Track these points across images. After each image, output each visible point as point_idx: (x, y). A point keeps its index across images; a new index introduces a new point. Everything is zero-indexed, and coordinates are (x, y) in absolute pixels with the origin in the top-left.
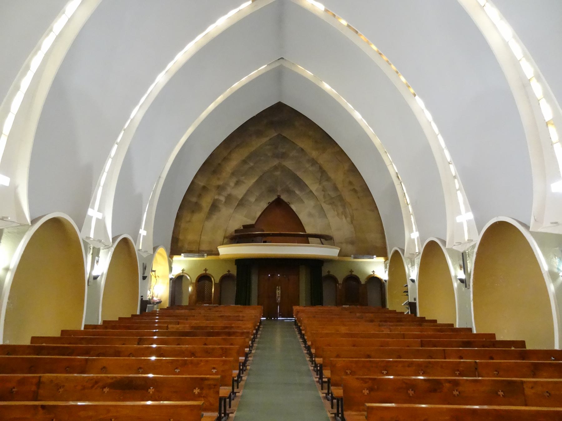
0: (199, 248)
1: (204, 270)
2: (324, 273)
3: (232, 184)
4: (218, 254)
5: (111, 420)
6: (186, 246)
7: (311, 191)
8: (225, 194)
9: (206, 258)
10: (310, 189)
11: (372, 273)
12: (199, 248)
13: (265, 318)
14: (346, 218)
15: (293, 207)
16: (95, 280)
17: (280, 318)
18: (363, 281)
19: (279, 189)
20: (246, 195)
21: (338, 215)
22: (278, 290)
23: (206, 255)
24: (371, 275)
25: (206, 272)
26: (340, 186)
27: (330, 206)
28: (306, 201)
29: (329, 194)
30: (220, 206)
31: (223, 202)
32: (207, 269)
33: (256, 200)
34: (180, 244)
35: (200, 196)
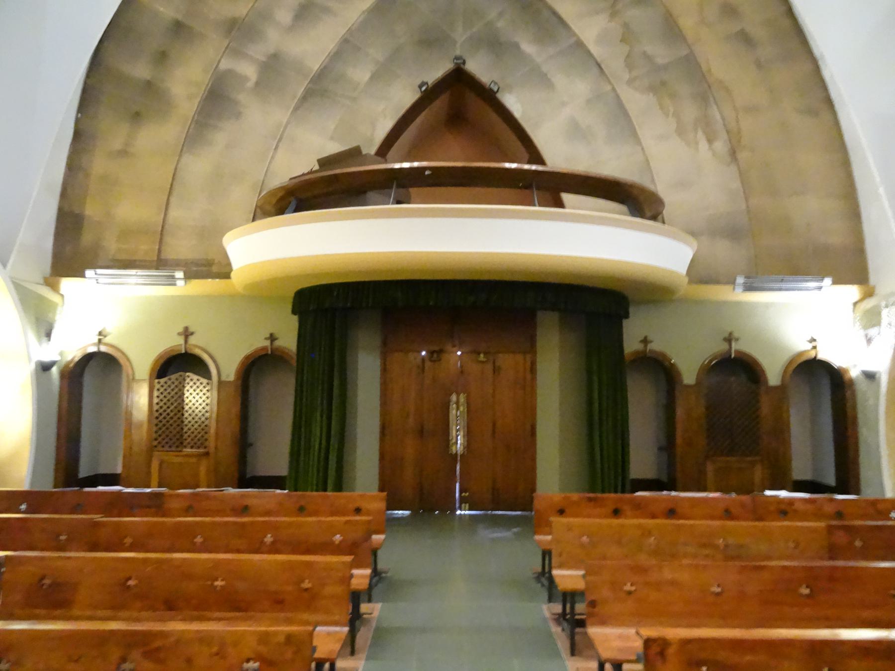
0: (160, 251)
1: (179, 334)
2: (631, 345)
3: (284, 16)
4: (225, 273)
5: (618, 667)
6: (112, 245)
7: (580, 45)
8: (259, 51)
9: (182, 287)
10: (575, 34)
11: (809, 346)
12: (160, 251)
13: (407, 513)
14: (710, 141)
15: (512, 102)
16: (47, 372)
17: (463, 512)
18: (774, 377)
19: (460, 35)
20: (337, 56)
21: (680, 131)
22: (458, 409)
23: (179, 274)
24: (801, 354)
25: (186, 341)
26: (687, 23)
27: (650, 99)
28: (559, 80)
29: (644, 53)
30: (242, 97)
31: (250, 84)
32: (191, 330)
33: (375, 77)
34: (87, 238)
35: (162, 58)
